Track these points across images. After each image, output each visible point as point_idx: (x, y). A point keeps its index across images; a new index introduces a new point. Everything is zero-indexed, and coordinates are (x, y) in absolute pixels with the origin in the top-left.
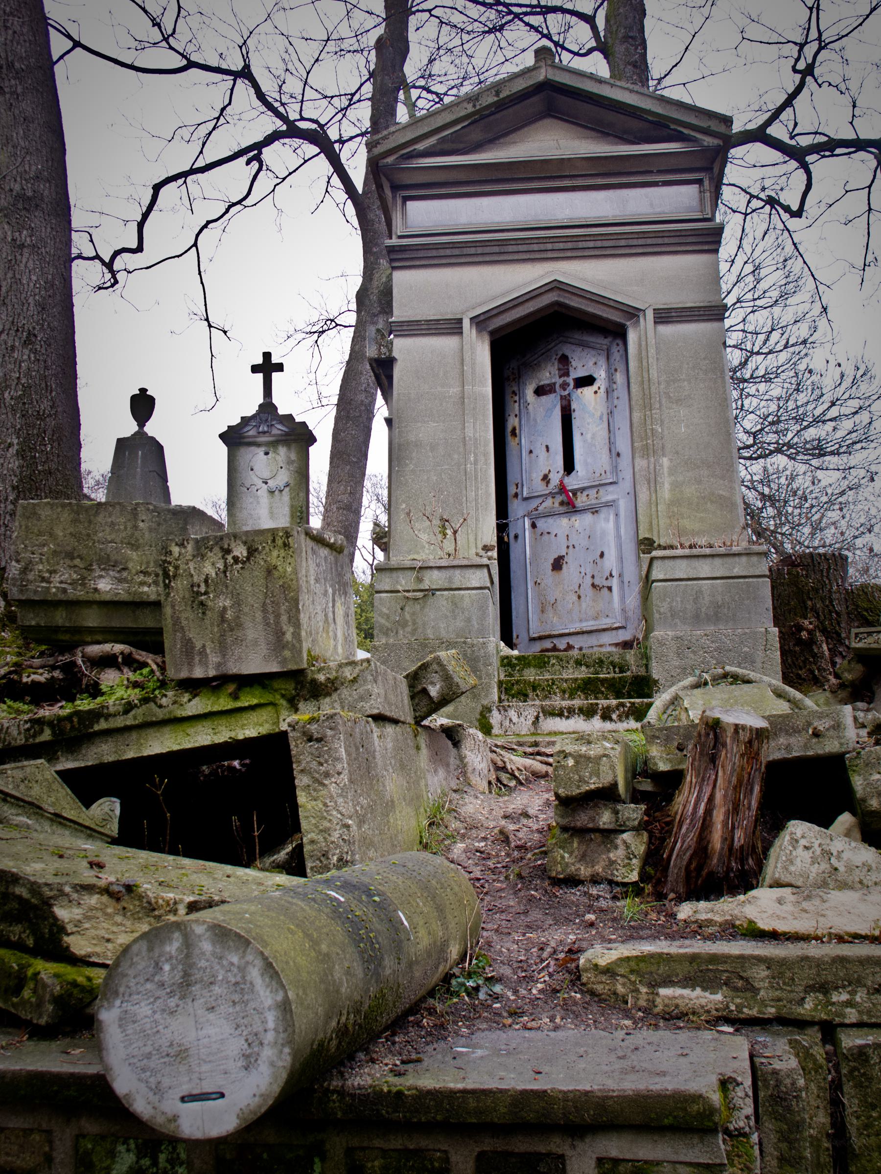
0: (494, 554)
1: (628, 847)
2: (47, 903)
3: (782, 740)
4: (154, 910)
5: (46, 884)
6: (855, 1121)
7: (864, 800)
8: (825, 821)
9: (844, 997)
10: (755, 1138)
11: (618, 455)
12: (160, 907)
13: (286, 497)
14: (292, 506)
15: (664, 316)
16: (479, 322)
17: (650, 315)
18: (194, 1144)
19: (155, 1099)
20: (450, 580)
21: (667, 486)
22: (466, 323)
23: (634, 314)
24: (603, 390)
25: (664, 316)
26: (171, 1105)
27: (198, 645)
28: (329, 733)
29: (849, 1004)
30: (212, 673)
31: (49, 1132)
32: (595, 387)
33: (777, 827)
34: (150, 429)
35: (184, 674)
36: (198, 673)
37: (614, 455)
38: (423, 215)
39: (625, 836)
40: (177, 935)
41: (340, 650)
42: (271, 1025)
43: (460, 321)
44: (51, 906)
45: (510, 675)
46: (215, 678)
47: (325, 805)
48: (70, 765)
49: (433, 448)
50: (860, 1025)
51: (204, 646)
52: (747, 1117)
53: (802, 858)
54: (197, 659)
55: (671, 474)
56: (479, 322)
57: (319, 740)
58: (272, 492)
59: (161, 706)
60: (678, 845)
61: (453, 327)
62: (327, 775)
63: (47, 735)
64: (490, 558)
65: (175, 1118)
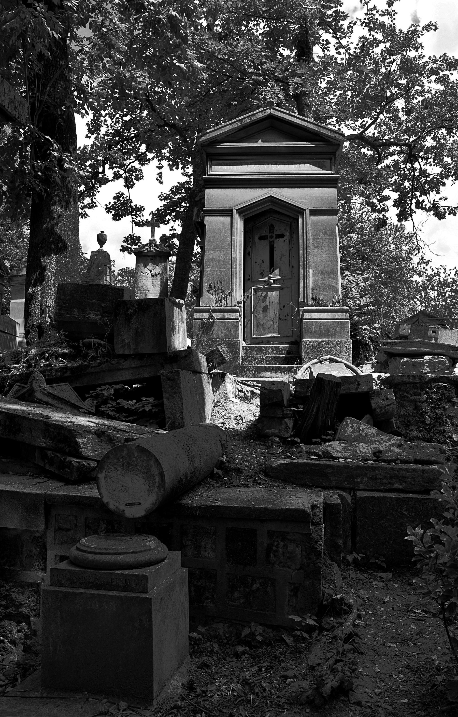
0: (242, 305)
1: (286, 424)
2: (74, 437)
3: (346, 386)
4: (112, 440)
5: (74, 430)
6: (359, 522)
7: (375, 410)
8: (360, 418)
9: (359, 480)
10: (323, 526)
11: (293, 267)
12: (114, 440)
13: (159, 278)
14: (161, 282)
15: (314, 212)
16: (240, 212)
17: (308, 212)
18: (129, 519)
19: (116, 504)
20: (224, 316)
21: (311, 281)
22: (234, 211)
23: (301, 211)
24: (288, 239)
25: (314, 212)
26: (122, 507)
27: (127, 342)
28: (176, 377)
29: (361, 482)
30: (132, 353)
31: (76, 517)
32: (284, 239)
33: (341, 420)
34: (105, 248)
35: (121, 352)
36: (127, 352)
37: (291, 267)
38: (217, 170)
39: (285, 420)
40: (125, 449)
41: (181, 345)
42: (157, 480)
43: (232, 210)
44: (75, 438)
45: (246, 354)
46: (133, 354)
47: (174, 404)
48: (78, 385)
49: (219, 261)
50: (364, 490)
51: (129, 342)
52: (320, 519)
53: (350, 430)
54: (126, 346)
55: (313, 276)
56: (240, 212)
57: (172, 380)
58: (152, 276)
59: (112, 364)
60: (305, 425)
61: (228, 213)
62: (175, 393)
63: (68, 374)
64: (240, 307)
65: (124, 511)
